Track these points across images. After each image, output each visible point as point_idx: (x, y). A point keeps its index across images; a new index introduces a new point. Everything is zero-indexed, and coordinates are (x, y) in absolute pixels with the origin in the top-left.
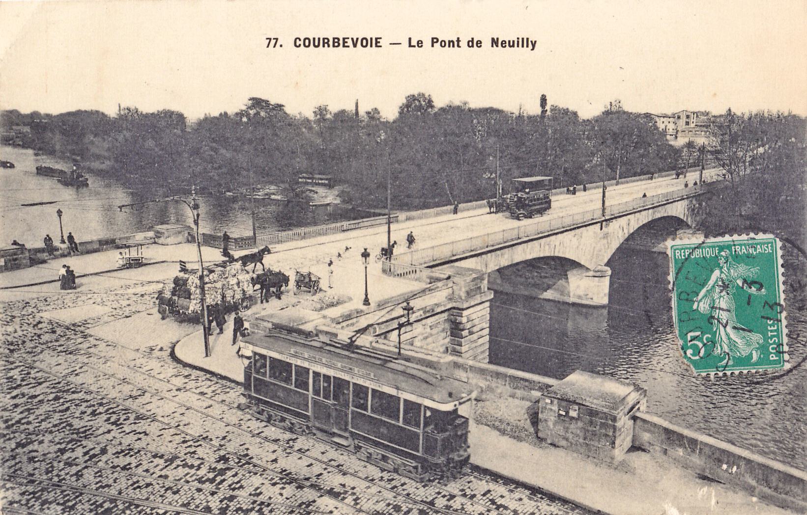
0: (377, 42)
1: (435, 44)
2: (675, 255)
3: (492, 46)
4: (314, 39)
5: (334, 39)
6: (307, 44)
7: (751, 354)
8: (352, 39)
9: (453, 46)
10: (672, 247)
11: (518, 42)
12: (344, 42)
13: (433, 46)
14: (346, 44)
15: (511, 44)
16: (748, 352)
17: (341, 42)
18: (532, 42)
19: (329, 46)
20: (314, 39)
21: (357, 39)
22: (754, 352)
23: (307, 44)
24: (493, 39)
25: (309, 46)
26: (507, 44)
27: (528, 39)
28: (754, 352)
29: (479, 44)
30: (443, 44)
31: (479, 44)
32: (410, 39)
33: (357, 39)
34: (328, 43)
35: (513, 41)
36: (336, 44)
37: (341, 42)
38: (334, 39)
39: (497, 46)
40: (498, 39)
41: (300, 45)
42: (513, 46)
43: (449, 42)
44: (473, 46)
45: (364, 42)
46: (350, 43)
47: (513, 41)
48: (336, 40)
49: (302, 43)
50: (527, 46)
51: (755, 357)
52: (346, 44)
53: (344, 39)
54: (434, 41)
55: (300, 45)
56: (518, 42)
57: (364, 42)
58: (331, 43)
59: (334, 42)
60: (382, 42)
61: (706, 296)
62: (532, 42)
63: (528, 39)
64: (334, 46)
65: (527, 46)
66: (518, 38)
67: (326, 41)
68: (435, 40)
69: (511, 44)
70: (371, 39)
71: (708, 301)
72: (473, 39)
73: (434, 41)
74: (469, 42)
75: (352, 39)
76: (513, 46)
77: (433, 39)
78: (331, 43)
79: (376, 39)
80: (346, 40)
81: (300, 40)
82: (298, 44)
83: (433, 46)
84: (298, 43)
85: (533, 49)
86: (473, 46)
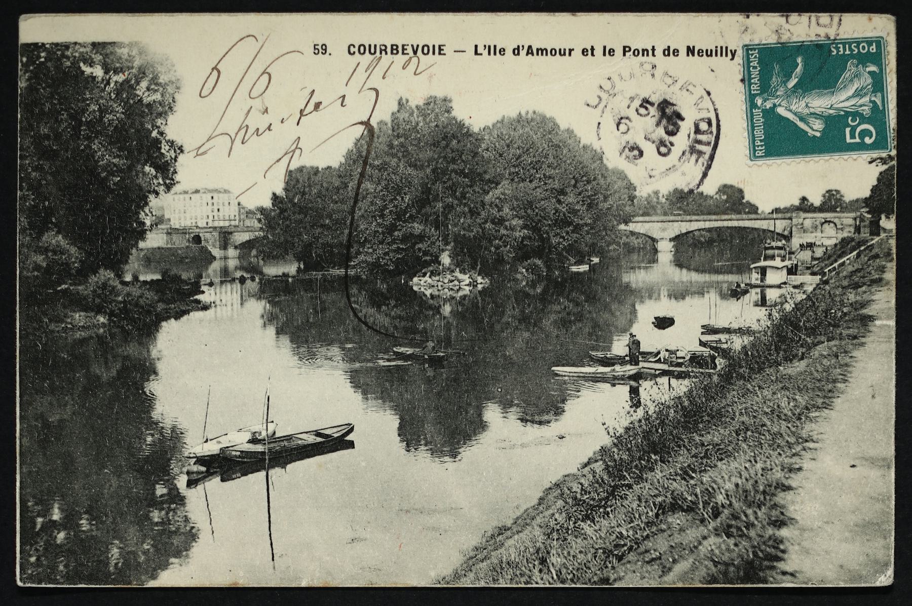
0: (440, 49)
1: (627, 54)
2: (762, 156)
3: (688, 55)
4: (370, 46)
5: (392, 46)
6: (362, 51)
7: (869, 73)
8: (412, 46)
9: (648, 55)
10: (752, 160)
11: (716, 51)
12: (403, 49)
13: (624, 55)
14: (405, 52)
15: (709, 53)
16: (867, 75)
17: (400, 49)
18: (731, 51)
19: (386, 53)
20: (370, 46)
21: (418, 46)
22: (868, 69)
23: (362, 51)
24: (688, 48)
25: (364, 53)
26: (704, 53)
27: (495, 46)
28: (868, 69)
29: (676, 52)
30: (636, 53)
31: (676, 52)
32: (476, 46)
33: (418, 46)
34: (385, 50)
35: (711, 51)
36: (395, 52)
37: (400, 49)
38: (392, 46)
39: (693, 55)
40: (694, 47)
41: (354, 52)
42: (711, 55)
43: (643, 50)
44: (669, 55)
45: (426, 49)
46: (409, 50)
47: (711, 51)
48: (395, 47)
49: (356, 50)
50: (727, 55)
51: (873, 68)
52: (405, 52)
53: (403, 46)
54: (626, 49)
55: (354, 52)
56: (716, 51)
57: (426, 49)
58: (389, 50)
59: (392, 49)
60: (446, 50)
61: (807, 124)
62: (731, 51)
63: (727, 48)
64: (392, 53)
65: (727, 55)
66: (716, 47)
67: (383, 48)
68: (627, 49)
69: (709, 53)
70: (434, 46)
71: (812, 120)
72: (669, 47)
73: (626, 49)
74: (514, 50)
75: (412, 46)
76: (711, 55)
77: (624, 47)
78: (389, 50)
79: (440, 46)
80: (405, 47)
81: (354, 46)
82: (352, 52)
83: (624, 55)
84: (352, 50)
85: (732, 59)
86: (669, 55)
